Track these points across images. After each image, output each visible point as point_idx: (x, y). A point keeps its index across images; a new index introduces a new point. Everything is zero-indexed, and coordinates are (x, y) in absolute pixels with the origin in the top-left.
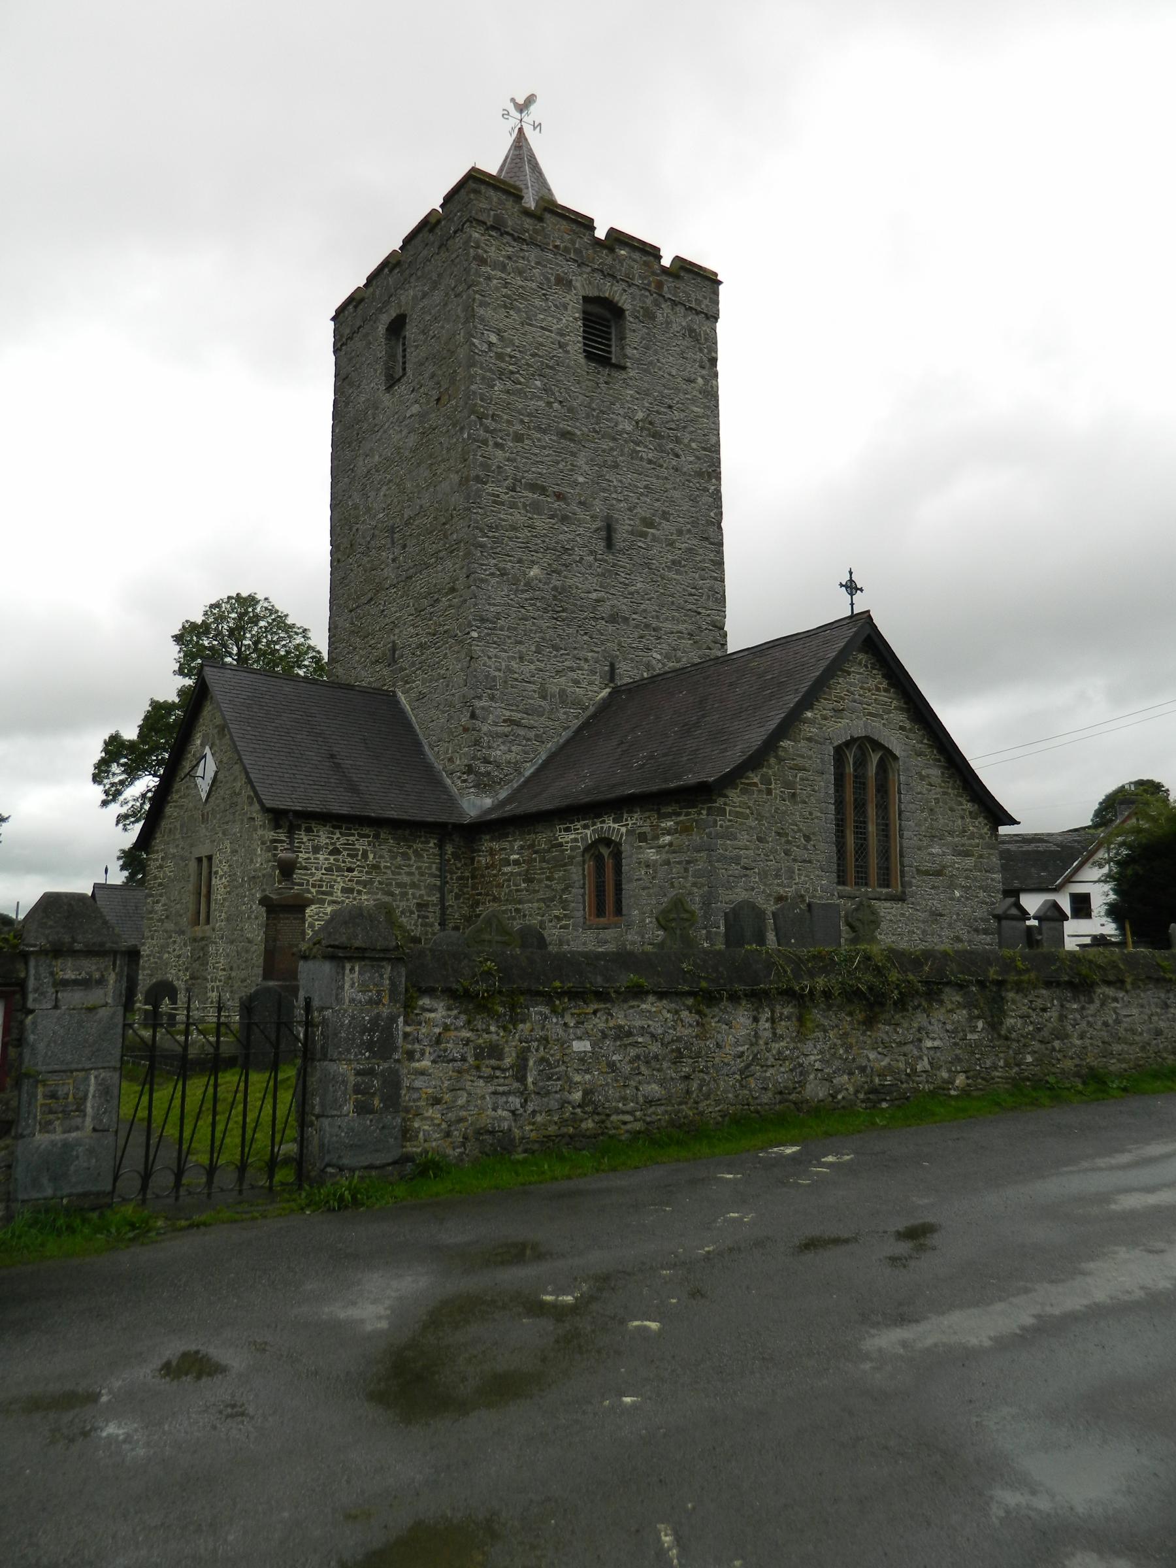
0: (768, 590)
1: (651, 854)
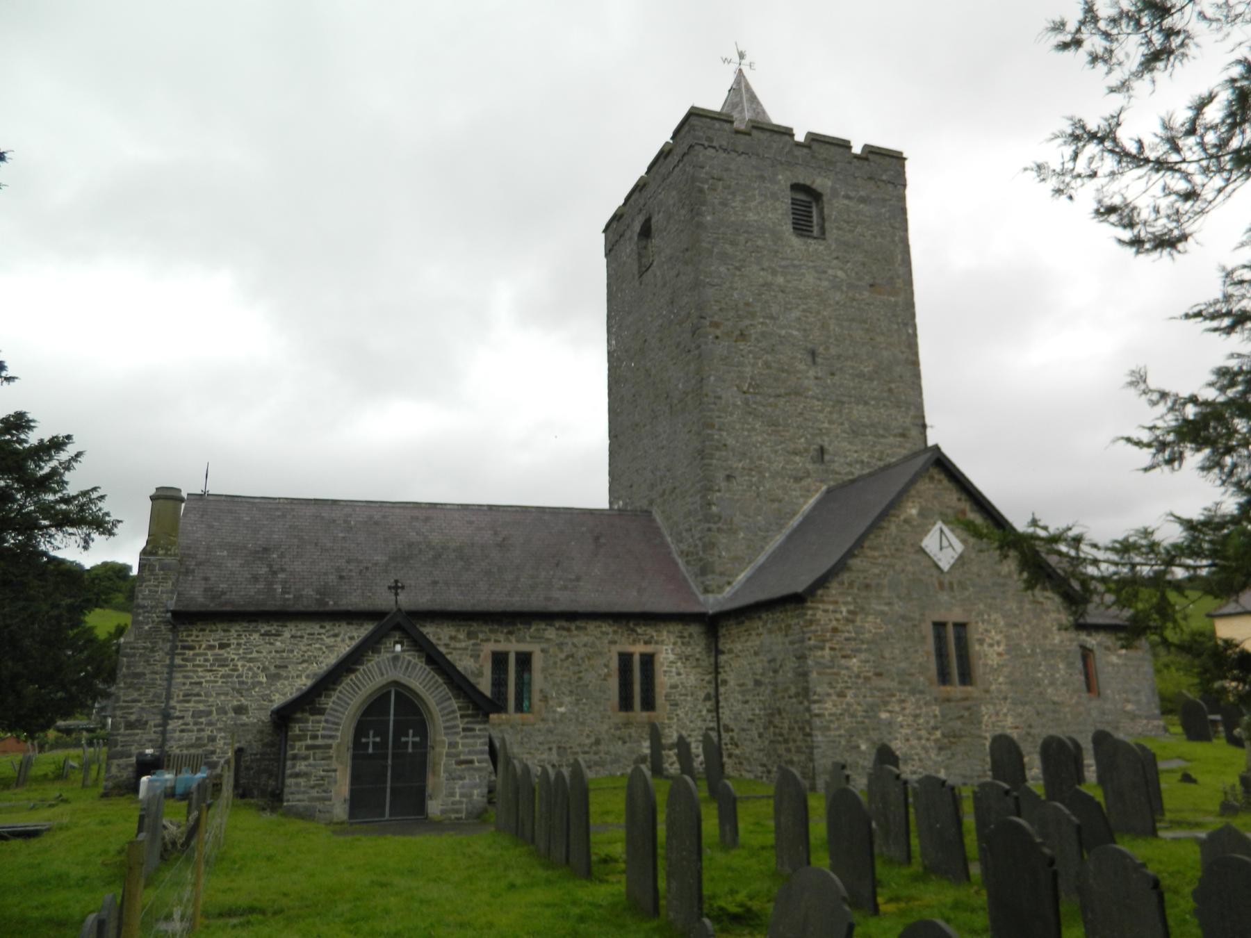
0: (930, 443)
1: (1114, 659)
